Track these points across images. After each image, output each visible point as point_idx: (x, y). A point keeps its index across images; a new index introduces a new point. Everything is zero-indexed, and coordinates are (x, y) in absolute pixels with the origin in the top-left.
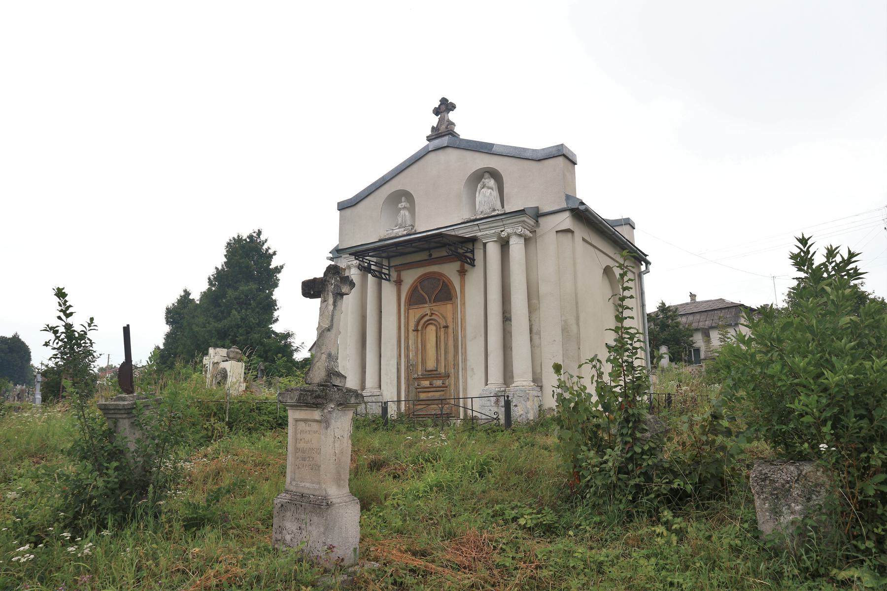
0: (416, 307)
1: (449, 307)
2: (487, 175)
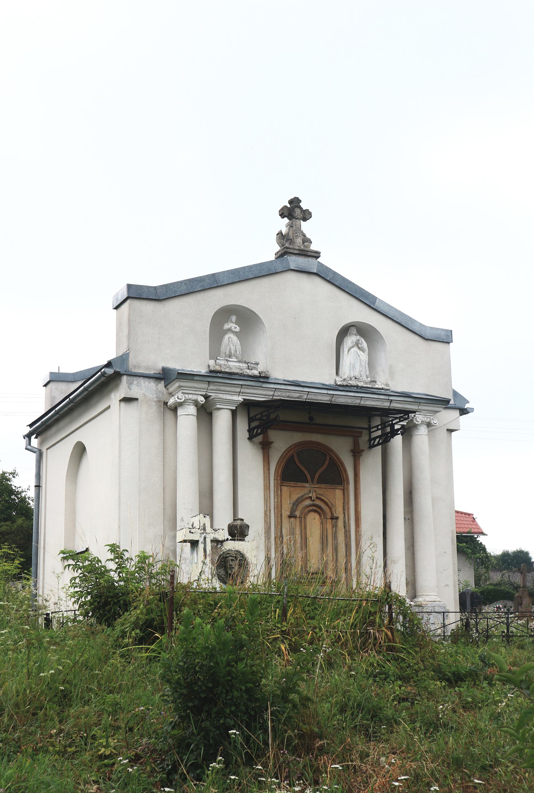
0: (292, 484)
1: (338, 493)
2: (353, 330)
